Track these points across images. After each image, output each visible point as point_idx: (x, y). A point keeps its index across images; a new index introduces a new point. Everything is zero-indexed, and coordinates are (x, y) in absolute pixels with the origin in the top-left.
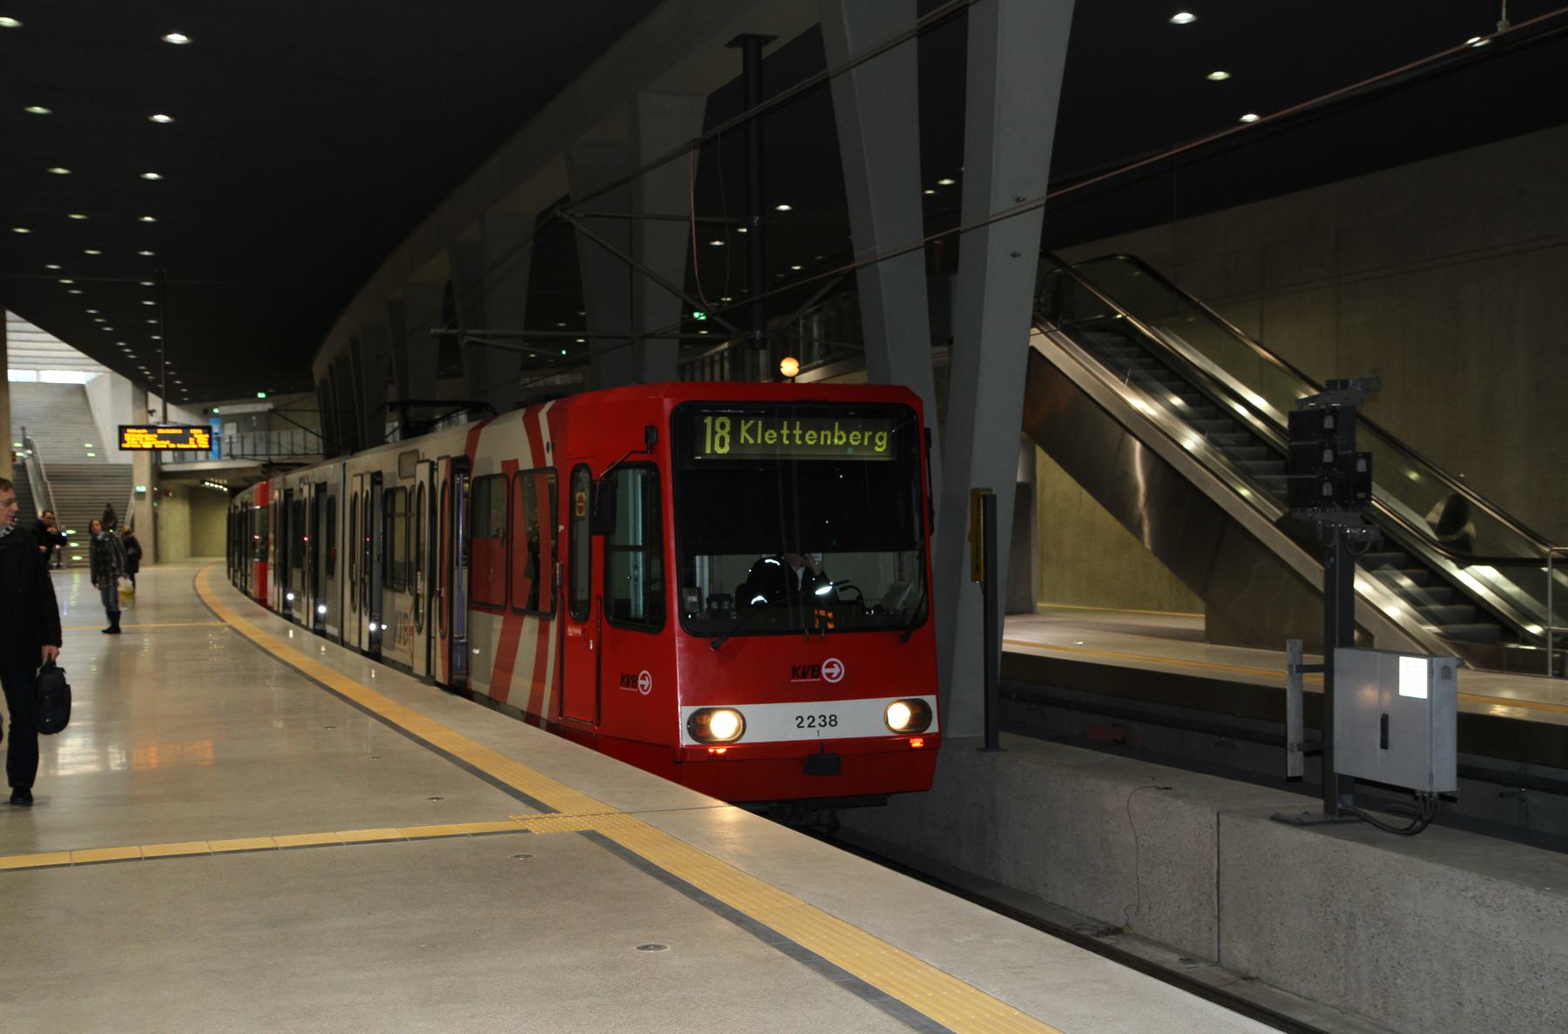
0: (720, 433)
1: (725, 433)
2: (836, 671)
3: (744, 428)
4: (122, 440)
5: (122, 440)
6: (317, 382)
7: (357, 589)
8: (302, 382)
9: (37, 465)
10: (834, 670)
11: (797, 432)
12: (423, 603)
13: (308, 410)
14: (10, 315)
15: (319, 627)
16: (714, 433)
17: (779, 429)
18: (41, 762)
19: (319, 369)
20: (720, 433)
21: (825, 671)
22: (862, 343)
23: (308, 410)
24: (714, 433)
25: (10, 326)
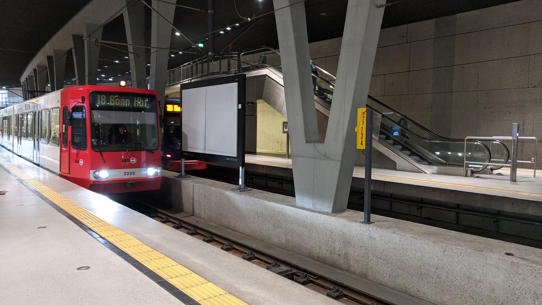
0: (103, 99)
1: (104, 99)
2: (134, 160)
8: (18, 85)
16: (101, 99)
19: (23, 79)
20: (103, 99)
21: (131, 160)
24: (101, 99)
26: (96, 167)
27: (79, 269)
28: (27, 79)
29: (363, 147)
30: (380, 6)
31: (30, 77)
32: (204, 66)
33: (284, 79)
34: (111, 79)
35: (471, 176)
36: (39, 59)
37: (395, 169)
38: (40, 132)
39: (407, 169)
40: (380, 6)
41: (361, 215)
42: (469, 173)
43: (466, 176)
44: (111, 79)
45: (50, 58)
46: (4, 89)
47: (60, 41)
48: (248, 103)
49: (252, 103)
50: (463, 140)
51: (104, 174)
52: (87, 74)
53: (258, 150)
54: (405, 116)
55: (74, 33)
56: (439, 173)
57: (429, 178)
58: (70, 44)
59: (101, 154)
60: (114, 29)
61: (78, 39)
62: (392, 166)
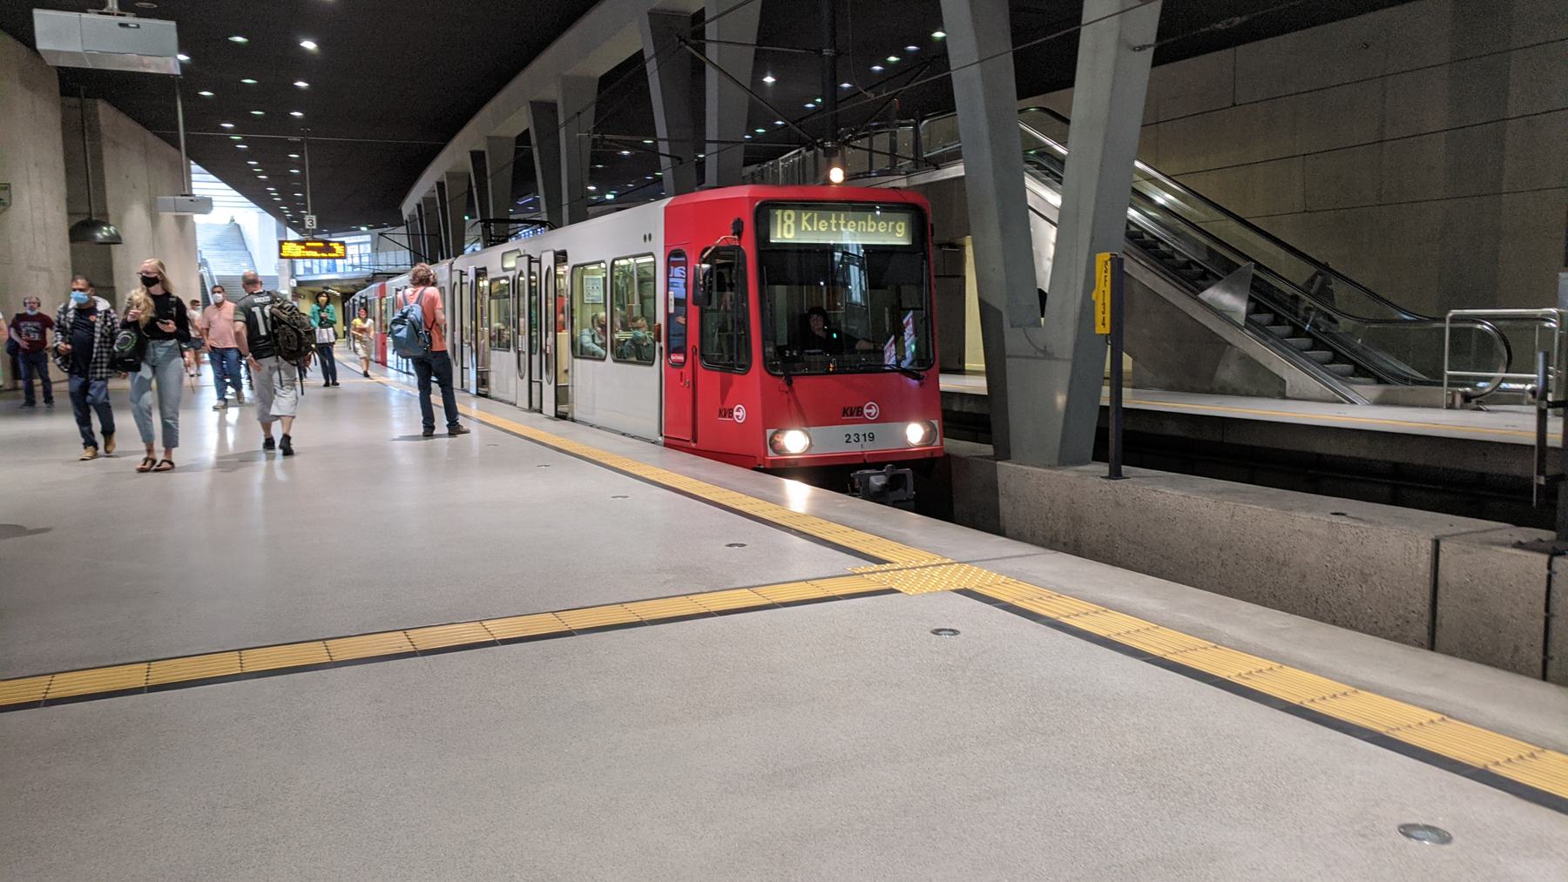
0: (788, 222)
1: (791, 222)
2: (873, 411)
3: (804, 218)
4: (281, 250)
5: (281, 250)
6: (405, 217)
7: (535, 358)
8: (397, 221)
9: (211, 277)
10: (872, 410)
11: (842, 222)
12: (525, 357)
13: (400, 234)
14: (195, 167)
15: (482, 390)
17: (829, 219)
18: (142, 70)
19: (408, 208)
20: (788, 222)
22: (571, 222)
23: (400, 234)
25: (194, 177)
26: (776, 418)
27: (1407, 830)
28: (419, 206)
29: (1107, 331)
30: (1142, 48)
31: (428, 201)
32: (899, 138)
33: (1024, 188)
34: (609, 197)
35: (1462, 408)
36: (452, 159)
37: (1283, 396)
38: (458, 325)
39: (1309, 395)
40: (1142, 48)
41: (1104, 468)
42: (1458, 399)
43: (1451, 407)
44: (609, 197)
45: (477, 157)
46: (364, 233)
47: (503, 118)
48: (940, 246)
49: (951, 245)
50: (1444, 320)
51: (795, 442)
52: (565, 200)
53: (968, 366)
54: (1326, 267)
55: (535, 98)
56: (1381, 402)
57: (1363, 412)
58: (521, 121)
59: (790, 383)
60: (625, 81)
61: (544, 111)
62: (1278, 389)
